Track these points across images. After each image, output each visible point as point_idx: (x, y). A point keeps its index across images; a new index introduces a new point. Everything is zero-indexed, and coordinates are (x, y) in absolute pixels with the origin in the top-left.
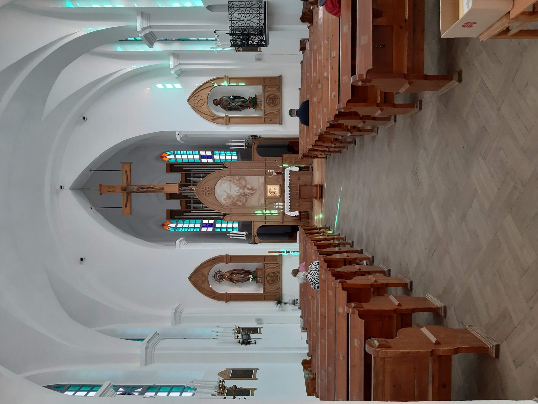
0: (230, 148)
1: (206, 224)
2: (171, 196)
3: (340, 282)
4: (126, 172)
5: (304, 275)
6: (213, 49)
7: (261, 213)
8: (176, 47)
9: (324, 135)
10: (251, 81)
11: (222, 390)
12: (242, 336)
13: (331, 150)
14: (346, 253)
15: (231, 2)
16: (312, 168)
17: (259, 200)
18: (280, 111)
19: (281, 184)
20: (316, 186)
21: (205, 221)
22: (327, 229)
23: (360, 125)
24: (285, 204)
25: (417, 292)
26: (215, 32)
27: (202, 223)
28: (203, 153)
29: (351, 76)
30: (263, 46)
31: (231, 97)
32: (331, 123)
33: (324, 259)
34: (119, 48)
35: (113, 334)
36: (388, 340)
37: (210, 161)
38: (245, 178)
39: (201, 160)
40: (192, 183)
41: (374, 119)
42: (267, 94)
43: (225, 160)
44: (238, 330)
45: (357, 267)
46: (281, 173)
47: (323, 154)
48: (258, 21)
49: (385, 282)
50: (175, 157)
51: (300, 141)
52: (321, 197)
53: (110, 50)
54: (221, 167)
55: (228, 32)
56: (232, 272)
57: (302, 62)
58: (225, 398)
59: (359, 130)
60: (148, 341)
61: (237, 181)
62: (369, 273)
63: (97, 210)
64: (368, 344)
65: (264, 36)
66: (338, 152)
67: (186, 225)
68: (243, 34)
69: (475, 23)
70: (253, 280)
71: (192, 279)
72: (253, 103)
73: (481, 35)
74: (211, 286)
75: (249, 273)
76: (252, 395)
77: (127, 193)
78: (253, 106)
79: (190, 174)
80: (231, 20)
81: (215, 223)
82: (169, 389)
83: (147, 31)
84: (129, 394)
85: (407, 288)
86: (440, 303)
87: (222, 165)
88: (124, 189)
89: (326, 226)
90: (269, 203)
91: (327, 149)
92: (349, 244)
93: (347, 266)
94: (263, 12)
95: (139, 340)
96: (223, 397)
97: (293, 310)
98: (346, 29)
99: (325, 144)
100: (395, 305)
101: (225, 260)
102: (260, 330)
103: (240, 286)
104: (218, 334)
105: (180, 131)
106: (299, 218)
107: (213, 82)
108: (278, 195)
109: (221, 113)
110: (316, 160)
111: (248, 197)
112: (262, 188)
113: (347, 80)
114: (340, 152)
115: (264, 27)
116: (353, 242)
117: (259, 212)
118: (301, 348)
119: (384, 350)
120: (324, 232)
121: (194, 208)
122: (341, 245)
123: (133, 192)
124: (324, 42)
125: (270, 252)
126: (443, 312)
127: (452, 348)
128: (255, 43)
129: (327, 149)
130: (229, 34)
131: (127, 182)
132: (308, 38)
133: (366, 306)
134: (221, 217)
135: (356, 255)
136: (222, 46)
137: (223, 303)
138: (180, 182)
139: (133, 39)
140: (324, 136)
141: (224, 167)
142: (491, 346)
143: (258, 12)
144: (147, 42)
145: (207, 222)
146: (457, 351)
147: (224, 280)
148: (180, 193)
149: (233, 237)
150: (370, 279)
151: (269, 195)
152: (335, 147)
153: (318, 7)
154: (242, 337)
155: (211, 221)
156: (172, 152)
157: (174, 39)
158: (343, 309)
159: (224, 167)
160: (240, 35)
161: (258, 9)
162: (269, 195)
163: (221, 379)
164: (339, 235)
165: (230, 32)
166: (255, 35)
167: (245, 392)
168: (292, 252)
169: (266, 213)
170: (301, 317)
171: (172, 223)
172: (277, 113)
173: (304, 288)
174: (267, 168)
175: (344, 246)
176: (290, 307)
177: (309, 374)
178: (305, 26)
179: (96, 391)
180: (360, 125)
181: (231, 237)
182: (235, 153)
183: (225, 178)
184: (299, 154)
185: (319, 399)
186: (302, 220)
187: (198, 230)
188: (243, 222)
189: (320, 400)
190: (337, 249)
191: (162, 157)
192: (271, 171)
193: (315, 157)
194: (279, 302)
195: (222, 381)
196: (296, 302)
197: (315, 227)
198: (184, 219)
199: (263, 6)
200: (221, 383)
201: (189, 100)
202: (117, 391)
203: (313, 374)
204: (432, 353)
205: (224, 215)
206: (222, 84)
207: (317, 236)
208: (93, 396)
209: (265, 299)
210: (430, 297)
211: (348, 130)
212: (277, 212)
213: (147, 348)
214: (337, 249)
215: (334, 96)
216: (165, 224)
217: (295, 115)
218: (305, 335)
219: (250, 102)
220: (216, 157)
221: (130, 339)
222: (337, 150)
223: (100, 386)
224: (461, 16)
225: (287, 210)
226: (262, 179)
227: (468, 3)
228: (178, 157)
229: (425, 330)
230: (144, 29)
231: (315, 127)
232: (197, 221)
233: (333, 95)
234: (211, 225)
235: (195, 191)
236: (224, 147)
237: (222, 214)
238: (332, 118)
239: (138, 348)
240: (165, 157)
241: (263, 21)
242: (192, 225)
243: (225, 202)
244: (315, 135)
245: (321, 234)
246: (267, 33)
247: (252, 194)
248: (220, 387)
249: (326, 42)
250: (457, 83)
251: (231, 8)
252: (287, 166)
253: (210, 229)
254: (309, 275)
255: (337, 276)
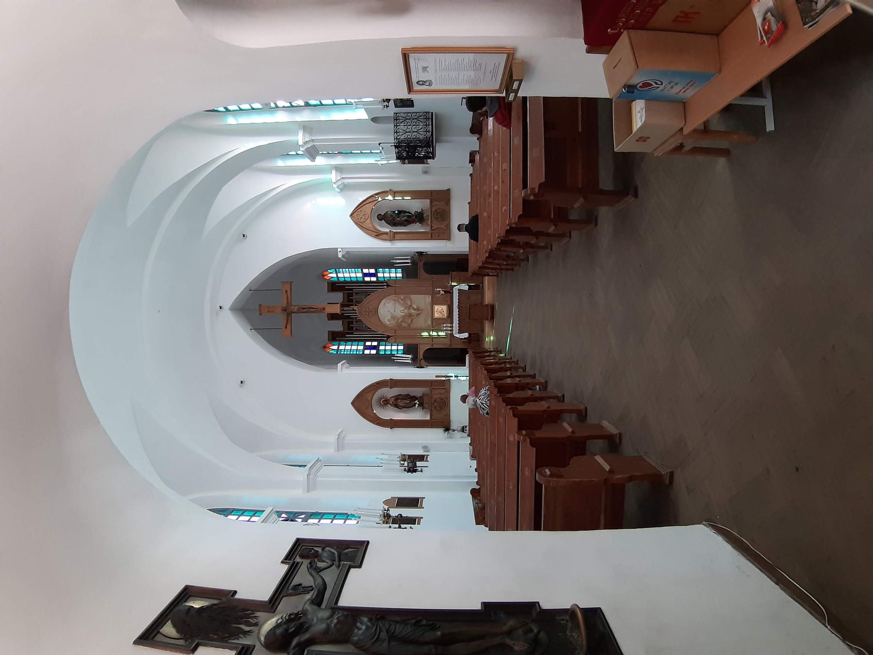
0: (395, 265)
1: (370, 346)
2: (333, 317)
3: (510, 409)
4: (286, 291)
5: (474, 401)
6: (377, 162)
7: (428, 334)
8: (339, 161)
9: (494, 251)
10: (417, 194)
11: (387, 518)
12: (408, 463)
13: (503, 268)
14: (519, 378)
15: (397, 114)
16: (482, 286)
17: (426, 321)
18: (448, 227)
19: (449, 303)
20: (487, 305)
21: (368, 344)
22: (499, 353)
23: (533, 241)
24: (454, 325)
25: (592, 419)
26: (379, 144)
27: (365, 345)
28: (366, 271)
29: (523, 190)
30: (430, 158)
31: (396, 212)
32: (502, 238)
33: (495, 384)
34: (280, 163)
35: (274, 460)
36: (561, 469)
37: (374, 279)
38: (410, 297)
39: (364, 279)
40: (354, 303)
41: (548, 235)
42: (434, 209)
43: (389, 278)
44: (404, 458)
45: (530, 392)
46: (449, 292)
47: (494, 271)
48: (425, 133)
49: (559, 408)
50: (337, 275)
51: (470, 258)
52: (492, 318)
53: (270, 165)
54: (385, 286)
55: (393, 144)
56: (397, 398)
57: (471, 175)
58: (390, 527)
59: (532, 246)
60: (310, 468)
61: (402, 300)
62: (542, 399)
63: (257, 332)
64: (539, 473)
65: (431, 148)
66: (508, 270)
67: (348, 347)
68: (408, 146)
69: (649, 138)
70: (419, 406)
71: (355, 404)
72: (419, 217)
73: (655, 150)
74: (374, 412)
75: (414, 398)
76: (419, 524)
77: (287, 313)
78: (420, 221)
79: (353, 293)
80: (397, 132)
81: (379, 345)
82: (332, 516)
83: (309, 145)
84: (292, 521)
85: (582, 415)
86: (616, 430)
87: (387, 284)
88: (284, 310)
89: (497, 348)
90: (437, 324)
91: (498, 267)
92: (521, 368)
93: (518, 392)
94: (430, 124)
95: (300, 466)
96: (388, 525)
97: (462, 437)
98: (517, 141)
99: (497, 262)
100: (568, 432)
101: (389, 384)
102: (427, 458)
103: (405, 412)
104: (382, 461)
105: (342, 248)
106: (468, 340)
107: (377, 197)
108: (445, 316)
109: (386, 229)
110: (486, 277)
111: (413, 317)
112: (429, 308)
113: (519, 194)
114: (513, 270)
115: (431, 139)
116: (525, 366)
117: (425, 334)
118: (470, 477)
119: (555, 479)
120: (495, 356)
121: (356, 329)
122: (513, 370)
123: (293, 313)
124: (494, 154)
125: (436, 377)
126: (618, 439)
127: (625, 476)
128: (422, 155)
129: (498, 267)
130: (394, 147)
131: (287, 302)
132: (478, 150)
133: (539, 434)
134: (385, 339)
135: (528, 380)
136: (388, 159)
137: (388, 430)
138: (342, 302)
139: (295, 153)
140: (495, 252)
141: (388, 286)
142: (665, 473)
143: (425, 124)
144: (309, 156)
145: (370, 345)
146: (631, 479)
147: (389, 405)
148: (342, 313)
149: (398, 361)
150: (543, 405)
151: (436, 315)
152: (507, 265)
153: (487, 118)
154: (408, 465)
155: (375, 344)
156: (334, 270)
157: (337, 152)
158: (513, 437)
159: (388, 286)
160: (406, 148)
161: (425, 120)
162: (436, 315)
163: (386, 507)
164: (511, 358)
165: (395, 144)
166: (422, 147)
167: (412, 521)
168: (460, 376)
169: (433, 335)
170: (470, 444)
171: (334, 345)
172: (445, 228)
173: (474, 413)
174: (434, 287)
175: (517, 371)
176: (459, 434)
177: (478, 503)
178: (474, 138)
179: (259, 516)
180: (533, 241)
181: (395, 360)
182: (400, 270)
183: (389, 297)
184: (468, 271)
185: (488, 528)
186: (472, 343)
187: (361, 353)
188: (408, 344)
189: (489, 530)
190: (508, 373)
191: (324, 276)
192: (438, 289)
193: (485, 275)
194: (447, 429)
195: (387, 509)
196: (465, 429)
197: (485, 350)
198: (346, 341)
199: (430, 117)
200: (386, 512)
201: (351, 215)
202: (279, 516)
203: (482, 503)
204: (606, 480)
205: (388, 337)
206: (386, 198)
207: (488, 360)
208: (255, 522)
209: (432, 426)
210: (605, 423)
211: (520, 247)
212: (444, 334)
213: (308, 475)
214: (508, 373)
215: (505, 211)
216: (327, 346)
217: (464, 230)
218: (474, 463)
219: (416, 216)
220: (380, 275)
221: (291, 465)
222: (509, 267)
223: (264, 511)
224: (635, 129)
225: (456, 332)
226: (428, 299)
227: (641, 118)
228: (340, 275)
229: (598, 458)
230: (306, 143)
231: (485, 243)
232: (360, 343)
233: (504, 209)
234: (374, 348)
235: (357, 311)
236: (386, 262)
237: (386, 336)
238: (503, 233)
239: (301, 475)
240: (327, 275)
241: (430, 133)
242: (354, 347)
243: (389, 323)
244: (486, 252)
245: (492, 358)
246: (434, 144)
247: (418, 315)
248: (384, 516)
249: (496, 154)
250: (633, 199)
251: (397, 120)
252: (456, 284)
253: (374, 352)
254: (478, 400)
255: (508, 402)
